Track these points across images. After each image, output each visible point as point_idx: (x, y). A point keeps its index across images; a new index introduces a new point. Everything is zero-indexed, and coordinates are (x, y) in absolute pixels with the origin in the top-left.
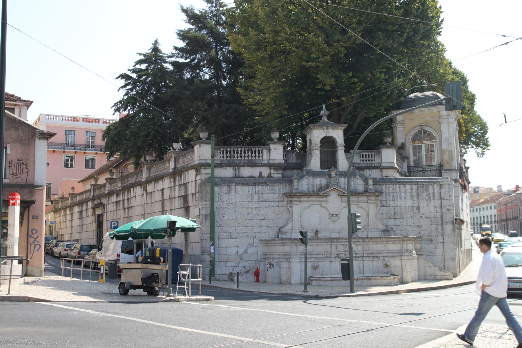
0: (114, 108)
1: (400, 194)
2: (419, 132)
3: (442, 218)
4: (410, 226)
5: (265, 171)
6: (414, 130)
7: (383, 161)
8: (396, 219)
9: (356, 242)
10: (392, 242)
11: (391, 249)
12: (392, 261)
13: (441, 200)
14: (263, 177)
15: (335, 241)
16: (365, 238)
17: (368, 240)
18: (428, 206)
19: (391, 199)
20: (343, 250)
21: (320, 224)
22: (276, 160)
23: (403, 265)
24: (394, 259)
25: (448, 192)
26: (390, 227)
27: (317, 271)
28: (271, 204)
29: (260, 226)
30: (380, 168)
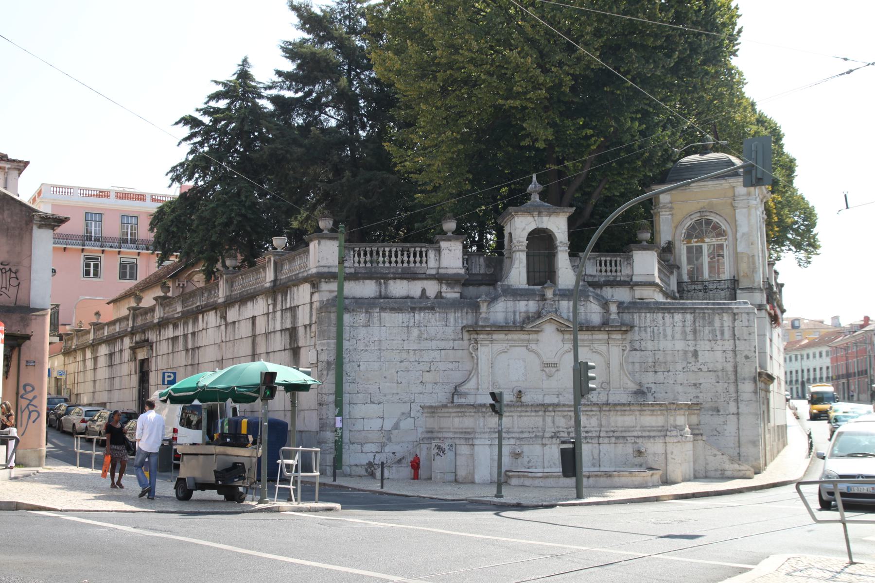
0: (171, 175)
1: (664, 330)
2: (699, 222)
3: (736, 371)
4: (681, 384)
5: (432, 288)
6: (689, 219)
8: (656, 372)
9: (586, 411)
10: (649, 412)
11: (648, 424)
12: (650, 444)
13: (735, 340)
14: (427, 298)
15: (551, 409)
19: (649, 338)
21: (526, 380)
22: (451, 268)
23: (669, 452)
24: (652, 440)
25: (747, 327)
26: (647, 385)
27: (520, 460)
28: (442, 345)
29: (422, 382)
30: (629, 284)
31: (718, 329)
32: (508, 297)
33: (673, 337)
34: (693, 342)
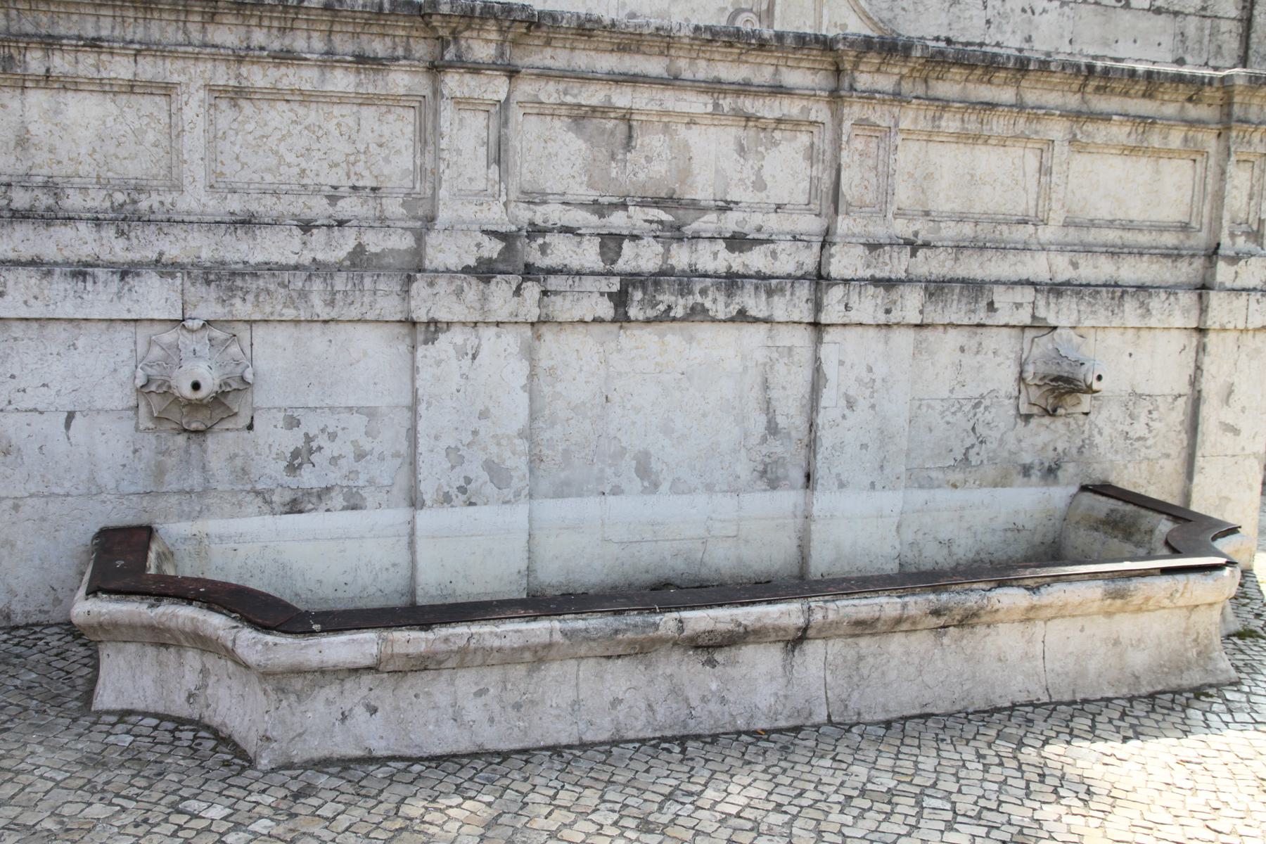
9: (744, 89)
10: (1119, 132)
11: (1103, 211)
15: (482, 48)
23: (1210, 387)
24: (1130, 312)
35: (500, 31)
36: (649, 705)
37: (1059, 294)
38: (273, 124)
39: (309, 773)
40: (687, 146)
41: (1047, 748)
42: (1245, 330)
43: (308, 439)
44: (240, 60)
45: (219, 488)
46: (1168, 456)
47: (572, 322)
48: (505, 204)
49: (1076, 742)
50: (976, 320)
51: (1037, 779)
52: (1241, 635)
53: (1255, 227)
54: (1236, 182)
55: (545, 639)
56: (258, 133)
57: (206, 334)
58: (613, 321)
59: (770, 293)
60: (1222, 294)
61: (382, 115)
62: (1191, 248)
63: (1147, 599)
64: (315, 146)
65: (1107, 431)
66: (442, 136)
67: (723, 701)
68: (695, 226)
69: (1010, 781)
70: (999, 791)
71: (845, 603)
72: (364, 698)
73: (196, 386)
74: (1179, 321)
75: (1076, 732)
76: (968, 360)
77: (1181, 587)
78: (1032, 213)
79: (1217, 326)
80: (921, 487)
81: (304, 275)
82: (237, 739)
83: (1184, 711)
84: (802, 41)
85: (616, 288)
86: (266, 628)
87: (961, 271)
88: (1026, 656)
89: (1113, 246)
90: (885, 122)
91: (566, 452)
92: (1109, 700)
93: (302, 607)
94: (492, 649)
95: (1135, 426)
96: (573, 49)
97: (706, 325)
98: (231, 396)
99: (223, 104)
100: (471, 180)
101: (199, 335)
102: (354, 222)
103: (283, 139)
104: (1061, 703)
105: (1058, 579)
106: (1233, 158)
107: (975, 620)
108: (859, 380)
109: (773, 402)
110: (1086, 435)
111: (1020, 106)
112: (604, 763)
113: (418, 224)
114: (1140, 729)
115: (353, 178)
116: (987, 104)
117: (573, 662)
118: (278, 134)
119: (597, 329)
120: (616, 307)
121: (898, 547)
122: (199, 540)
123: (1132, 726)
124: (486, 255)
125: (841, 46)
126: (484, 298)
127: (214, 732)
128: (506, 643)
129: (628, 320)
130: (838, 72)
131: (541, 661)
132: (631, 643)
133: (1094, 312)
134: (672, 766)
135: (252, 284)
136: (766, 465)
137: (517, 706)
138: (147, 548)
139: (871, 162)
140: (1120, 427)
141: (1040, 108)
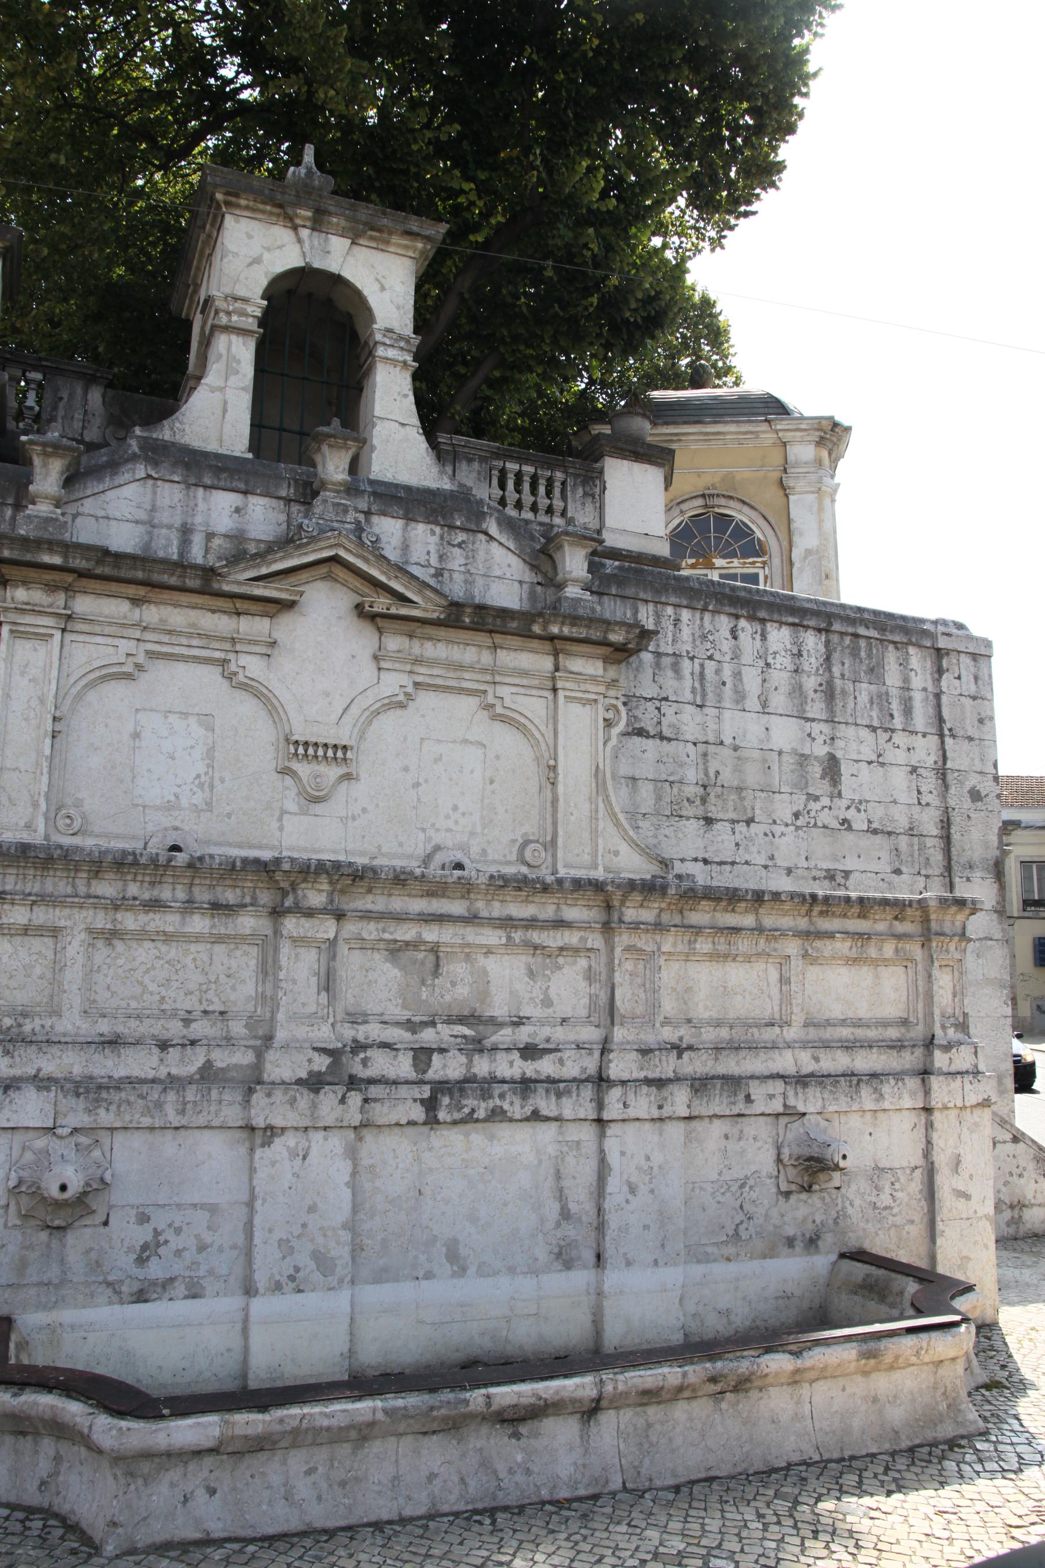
1: (737, 675)
4: (789, 871)
7: (609, 522)
8: (709, 821)
9: (532, 923)
10: (842, 946)
11: (836, 1011)
13: (941, 736)
15: (315, 897)
16: (632, 886)
17: (647, 915)
18: (879, 761)
19: (688, 696)
20: (396, 1011)
21: (209, 804)
23: (941, 1159)
24: (867, 1098)
25: (974, 698)
31: (894, 692)
32: (164, 471)
33: (764, 704)
34: (825, 728)
35: (331, 883)
36: (462, 1479)
37: (805, 1085)
38: (140, 959)
39: (151, 1558)
40: (485, 973)
41: (821, 1505)
42: (963, 1108)
43: (157, 1233)
44: (116, 908)
45: (75, 1280)
46: (912, 1222)
47: (389, 1126)
48: (333, 1025)
49: (846, 1499)
50: (736, 1111)
51: (811, 1535)
52: (988, 1387)
53: (961, 1020)
54: (941, 983)
55: (369, 1417)
56: (127, 968)
57: (73, 1140)
58: (425, 1123)
59: (559, 1095)
60: (941, 1078)
61: (232, 951)
62: (911, 1039)
63: (897, 1357)
64: (174, 977)
65: (857, 1202)
66: (280, 968)
67: (528, 1472)
68: (494, 1039)
69: (787, 1539)
70: (778, 1549)
71: (633, 1374)
72: (205, 1479)
73: (63, 1188)
74: (907, 1102)
75: (845, 1488)
76: (733, 1146)
77: (924, 1345)
78: (777, 1016)
79: (940, 1105)
80: (699, 1262)
81: (160, 1087)
82: (84, 1525)
83: (940, 1463)
84: (578, 884)
85: (427, 1094)
86: (120, 1414)
87: (721, 1069)
88: (796, 1417)
89: (847, 1041)
90: (649, 948)
91: (384, 1242)
92: (873, 1455)
93: (155, 1393)
94: (321, 1428)
95: (882, 1196)
96: (390, 895)
97: (505, 1125)
98: (90, 1196)
99: (100, 944)
100: (304, 1004)
101: (67, 1141)
102: (204, 1042)
103: (146, 972)
104: (831, 1461)
105: (817, 1343)
106: (936, 964)
107: (748, 1385)
108: (639, 1168)
109: (566, 1191)
110: (839, 1207)
111: (760, 929)
112: (422, 1537)
113: (259, 1043)
114: (901, 1483)
115: (205, 1003)
116: (733, 928)
117: (393, 1439)
118: (143, 968)
119: (410, 1131)
120: (427, 1111)
121: (682, 1318)
122: (52, 1329)
123: (895, 1480)
124: (316, 1068)
125: (609, 888)
126: (314, 1106)
127: (63, 1519)
128: (334, 1422)
129: (438, 1122)
130: (609, 907)
131: (365, 1438)
132: (445, 1419)
133: (836, 1099)
134: (484, 1538)
135: (115, 1096)
136: (561, 1248)
137: (343, 1484)
138: (7, 1339)
139: (639, 981)
140: (869, 1199)
141: (776, 930)
